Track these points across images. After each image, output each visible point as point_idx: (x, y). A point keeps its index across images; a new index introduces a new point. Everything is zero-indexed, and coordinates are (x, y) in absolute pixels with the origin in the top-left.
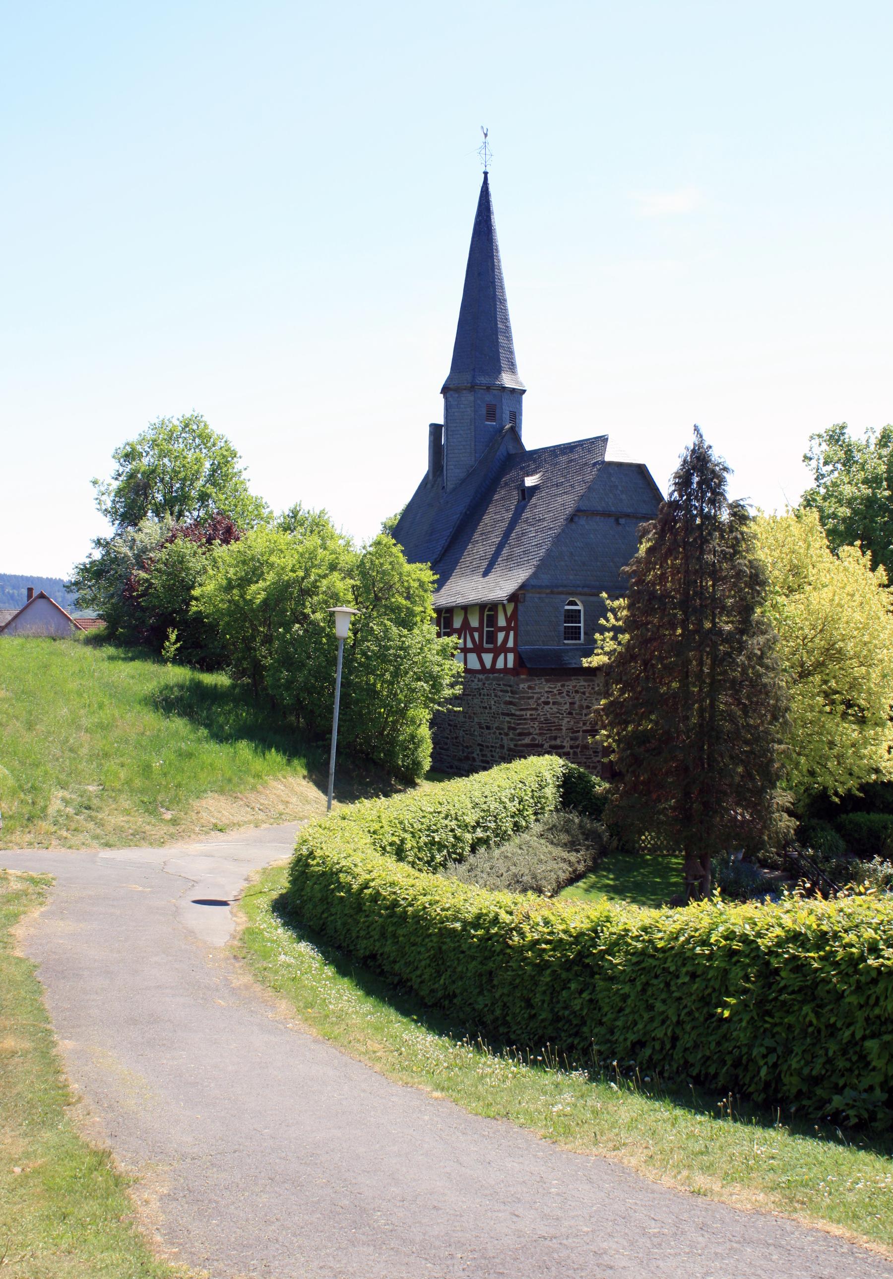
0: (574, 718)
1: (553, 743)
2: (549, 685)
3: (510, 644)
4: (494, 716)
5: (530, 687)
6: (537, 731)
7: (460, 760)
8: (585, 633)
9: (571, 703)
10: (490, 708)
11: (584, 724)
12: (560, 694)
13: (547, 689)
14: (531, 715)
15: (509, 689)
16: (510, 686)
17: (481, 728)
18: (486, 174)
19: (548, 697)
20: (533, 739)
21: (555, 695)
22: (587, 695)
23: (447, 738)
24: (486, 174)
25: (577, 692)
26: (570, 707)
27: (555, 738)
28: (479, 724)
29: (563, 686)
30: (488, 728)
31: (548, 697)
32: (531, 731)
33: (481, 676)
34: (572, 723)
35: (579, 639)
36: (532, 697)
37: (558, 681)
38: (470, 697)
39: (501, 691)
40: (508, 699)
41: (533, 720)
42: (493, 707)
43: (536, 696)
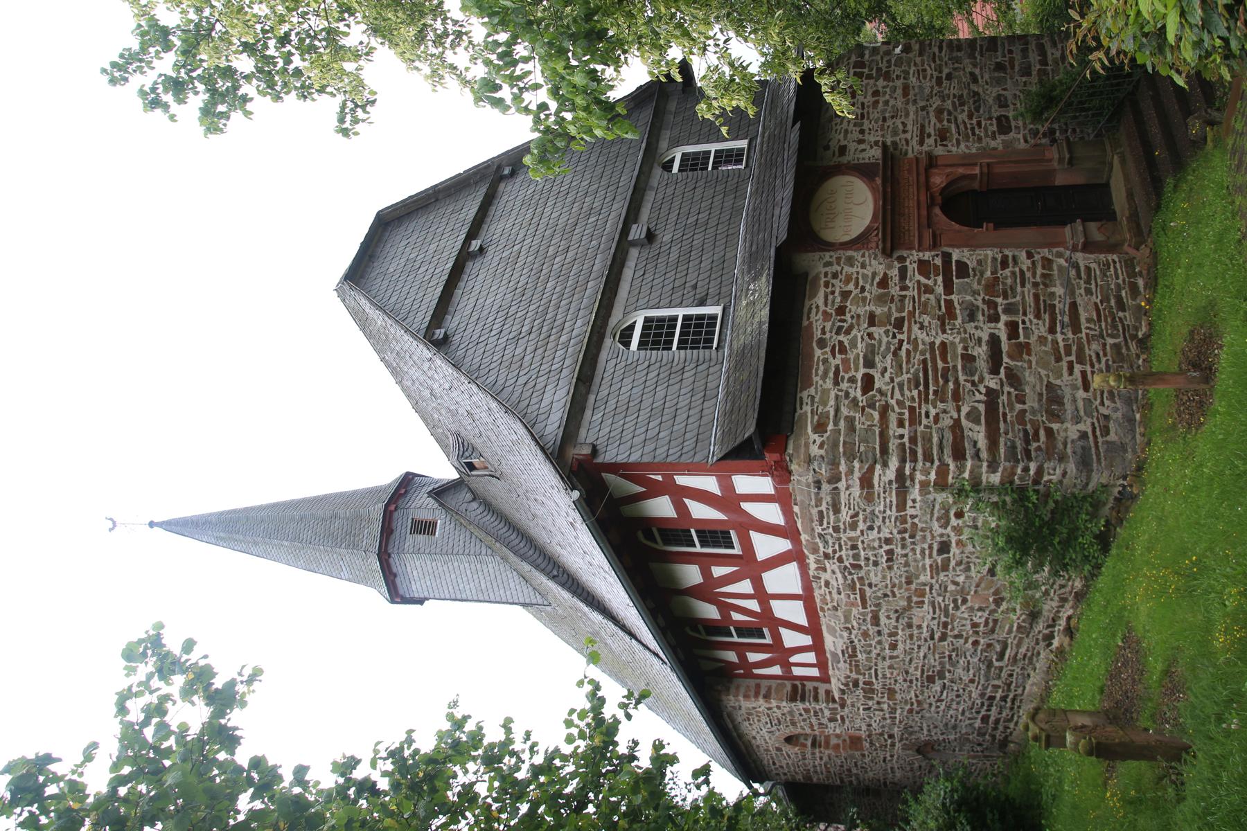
0: (912, 314)
1: (982, 364)
2: (815, 379)
3: (709, 483)
4: (909, 531)
5: (820, 428)
6: (950, 405)
7: (1034, 616)
8: (702, 303)
9: (872, 323)
10: (888, 541)
11: (929, 290)
12: (843, 350)
13: (829, 384)
14: (901, 424)
15: (826, 487)
16: (818, 484)
17: (945, 567)
18: (152, 524)
19: (852, 380)
20: (973, 416)
21: (846, 362)
22: (851, 287)
23: (976, 643)
24: (152, 524)
25: (841, 311)
26: (882, 324)
27: (969, 359)
28: (936, 570)
29: (822, 343)
30: (944, 548)
31: (852, 380)
32: (946, 422)
33: (811, 560)
34: (926, 319)
35: (714, 317)
36: (850, 421)
37: (811, 355)
38: (868, 591)
39: (837, 511)
40: (856, 491)
41: (914, 419)
42: (885, 533)
43: (845, 411)
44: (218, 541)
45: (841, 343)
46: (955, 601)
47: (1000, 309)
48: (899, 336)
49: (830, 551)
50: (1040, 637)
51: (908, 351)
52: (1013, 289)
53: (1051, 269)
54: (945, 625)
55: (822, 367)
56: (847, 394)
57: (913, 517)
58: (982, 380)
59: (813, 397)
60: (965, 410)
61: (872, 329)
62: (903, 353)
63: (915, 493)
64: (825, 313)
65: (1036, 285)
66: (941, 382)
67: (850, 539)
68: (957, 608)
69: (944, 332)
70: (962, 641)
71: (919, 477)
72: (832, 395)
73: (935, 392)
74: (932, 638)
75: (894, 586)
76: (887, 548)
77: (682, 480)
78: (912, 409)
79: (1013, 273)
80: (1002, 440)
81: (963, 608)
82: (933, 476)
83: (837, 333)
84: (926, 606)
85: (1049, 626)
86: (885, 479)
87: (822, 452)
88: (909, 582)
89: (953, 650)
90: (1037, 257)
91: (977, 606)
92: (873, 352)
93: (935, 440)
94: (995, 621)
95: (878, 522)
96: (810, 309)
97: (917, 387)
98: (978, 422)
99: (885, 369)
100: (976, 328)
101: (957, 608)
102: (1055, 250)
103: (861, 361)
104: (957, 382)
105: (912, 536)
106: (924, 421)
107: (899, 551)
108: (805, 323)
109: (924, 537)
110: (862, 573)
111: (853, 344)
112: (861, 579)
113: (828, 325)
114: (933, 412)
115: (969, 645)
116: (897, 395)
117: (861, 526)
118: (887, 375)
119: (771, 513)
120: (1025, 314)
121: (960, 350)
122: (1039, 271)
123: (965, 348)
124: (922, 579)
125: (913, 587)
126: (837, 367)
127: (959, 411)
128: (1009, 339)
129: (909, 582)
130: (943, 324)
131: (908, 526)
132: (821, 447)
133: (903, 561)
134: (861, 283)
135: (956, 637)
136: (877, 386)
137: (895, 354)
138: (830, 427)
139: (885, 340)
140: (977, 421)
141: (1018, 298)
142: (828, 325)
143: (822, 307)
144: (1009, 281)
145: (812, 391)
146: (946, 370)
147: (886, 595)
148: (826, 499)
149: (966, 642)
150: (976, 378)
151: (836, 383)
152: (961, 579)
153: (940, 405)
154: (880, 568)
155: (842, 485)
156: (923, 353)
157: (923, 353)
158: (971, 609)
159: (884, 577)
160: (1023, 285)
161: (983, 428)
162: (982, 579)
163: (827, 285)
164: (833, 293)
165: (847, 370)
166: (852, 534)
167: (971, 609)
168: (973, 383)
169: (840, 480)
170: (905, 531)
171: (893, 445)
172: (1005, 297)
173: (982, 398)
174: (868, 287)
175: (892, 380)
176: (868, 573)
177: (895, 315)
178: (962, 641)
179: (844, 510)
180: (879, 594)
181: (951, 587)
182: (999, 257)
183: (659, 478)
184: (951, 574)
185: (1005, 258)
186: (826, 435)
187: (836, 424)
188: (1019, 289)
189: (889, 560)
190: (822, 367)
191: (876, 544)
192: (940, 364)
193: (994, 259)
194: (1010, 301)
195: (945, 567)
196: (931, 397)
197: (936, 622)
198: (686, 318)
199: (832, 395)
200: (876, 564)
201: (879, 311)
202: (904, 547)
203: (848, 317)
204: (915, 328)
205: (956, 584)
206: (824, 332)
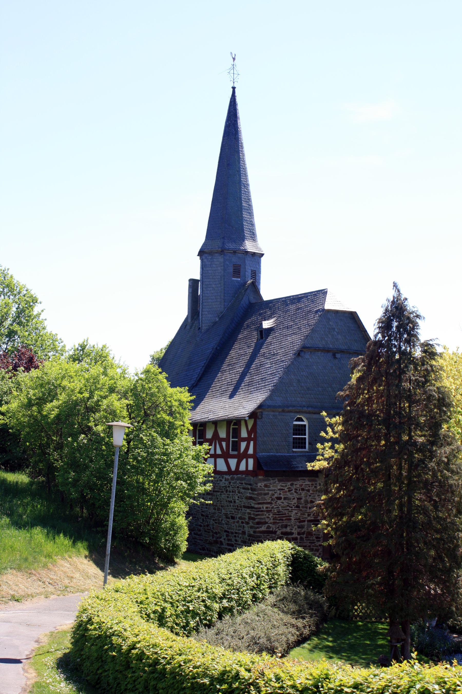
0: (301, 510)
1: (284, 530)
3: (251, 451)
5: (266, 486)
6: (272, 521)
9: (298, 499)
10: (235, 502)
11: (309, 515)
12: (289, 491)
13: (279, 487)
14: (267, 508)
15: (249, 487)
16: (250, 485)
17: (227, 518)
19: (280, 494)
20: (269, 527)
21: (286, 492)
22: (311, 492)
23: (201, 526)
25: (303, 490)
27: (286, 526)
28: (226, 515)
29: (292, 485)
30: (233, 518)
31: (280, 494)
33: (227, 477)
34: (299, 514)
35: (305, 448)
36: (268, 494)
37: (288, 481)
38: (219, 493)
39: (244, 488)
40: (248, 495)
41: (268, 511)
42: (237, 501)
43: (270, 492)
44: (231, 102)
45: (292, 490)
46: (216, 520)
47: (302, 536)
48: (293, 507)
49: (232, 484)
50: (204, 546)
51: (288, 509)
52: (309, 540)
53: (315, 551)
54: (207, 516)
55: (284, 485)
56: (276, 493)
57: (242, 510)
58: (279, 530)
59: (275, 483)
60: (271, 525)
61: (296, 499)
62: (288, 508)
63: (248, 511)
64: (302, 485)
65: (310, 546)
66: (279, 519)
67: (235, 491)
68: (213, 520)
69: (295, 519)
70: (201, 521)
71: (252, 512)
72: (276, 488)
73: (276, 517)
74: (202, 512)
75: (221, 501)
76: (233, 501)
77: (252, 443)
78: (271, 511)
79: (314, 540)
80: (262, 535)
81: (213, 522)
82: (252, 516)
83: (295, 489)
84: (214, 511)
85: (207, 549)
86: (252, 503)
87: (259, 487)
88: (222, 506)
89: (198, 518)
90: (319, 547)
91: (214, 526)
92: (288, 499)
93: (262, 517)
94: (209, 532)
95: (240, 499)
96: (304, 480)
97: (278, 512)
98: (267, 528)
99: (283, 503)
100: (296, 529)
101: (213, 520)
102: (322, 553)
103: (286, 496)
104: (278, 523)
105: (236, 509)
106: (267, 514)
107: (232, 504)
108: (299, 479)
109: (236, 512)
110: (225, 492)
111: (292, 494)
112: (223, 492)
113: (298, 486)
114: (270, 516)
115: (200, 524)
116: (275, 507)
117: (239, 495)
118: (281, 504)
119: (242, 467)
120: (300, 543)
121: (288, 524)
122: (315, 548)
123: (289, 525)
124: (223, 511)
125: (221, 507)
126: (284, 489)
127: (271, 523)
128: (292, 538)
129: (222, 506)
130: (297, 519)
131: (239, 508)
132: (260, 486)
133: (229, 505)
134: (312, 495)
135: (203, 520)
136: (278, 501)
137: (288, 506)
138: (266, 489)
139: (292, 503)
140: (267, 528)
141: (305, 541)
142: (298, 486)
143: (304, 484)
144: (311, 539)
145: (277, 482)
146: (283, 520)
147: (217, 499)
148: (247, 486)
149: (201, 523)
150: (280, 528)
151: (279, 489)
152: (223, 522)
153: (272, 518)
154: (226, 498)
155: (250, 491)
156: (288, 514)
157: (288, 514)
158: (213, 525)
159: (223, 499)
160: (310, 543)
161: (265, 529)
162: (223, 528)
163: (312, 485)
164: (309, 487)
165: (283, 492)
166: (237, 492)
167: (213, 525)
168: (278, 527)
169: (252, 491)
170: (238, 506)
171: (261, 506)
172: (305, 537)
173: (274, 530)
174: (311, 497)
175: (280, 505)
176: (225, 494)
177: (301, 506)
178: (201, 521)
179: (244, 490)
180: (218, 497)
181: (220, 519)
182: (320, 536)
183: (252, 436)
184: (225, 519)
185: (320, 538)
186: (264, 488)
187: (267, 490)
188: (309, 541)
189: (229, 501)
190: (284, 485)
191: (234, 498)
192: (284, 518)
193: (319, 535)
194: (305, 539)
195: (227, 518)
196: (275, 516)
197: (208, 513)
198: (305, 438)
199: (276, 488)
200: (228, 497)
201: (302, 501)
202: (233, 506)
203: (301, 491)
204: (296, 511)
205: (222, 520)
206: (295, 485)
